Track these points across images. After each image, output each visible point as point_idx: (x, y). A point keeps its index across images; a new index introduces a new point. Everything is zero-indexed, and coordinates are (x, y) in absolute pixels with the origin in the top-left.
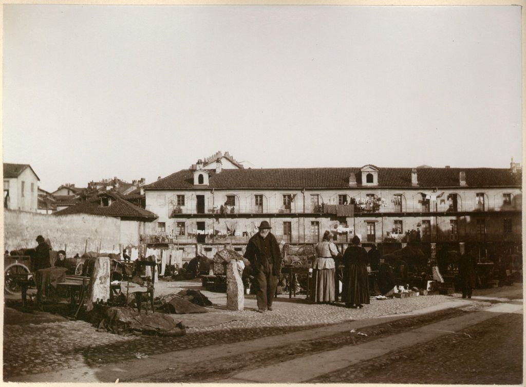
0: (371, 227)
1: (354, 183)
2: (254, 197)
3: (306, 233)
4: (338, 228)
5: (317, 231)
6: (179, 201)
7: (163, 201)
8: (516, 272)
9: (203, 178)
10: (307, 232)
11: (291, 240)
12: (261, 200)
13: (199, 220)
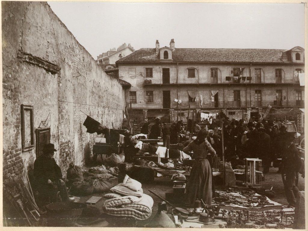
0: (298, 95)
1: (286, 60)
2: (210, 70)
3: (251, 100)
4: (186, 100)
5: (259, 98)
6: (147, 73)
7: (134, 73)
8: (211, 137)
9: (164, 54)
10: (252, 99)
11: (240, 106)
12: (216, 73)
13: (165, 89)
